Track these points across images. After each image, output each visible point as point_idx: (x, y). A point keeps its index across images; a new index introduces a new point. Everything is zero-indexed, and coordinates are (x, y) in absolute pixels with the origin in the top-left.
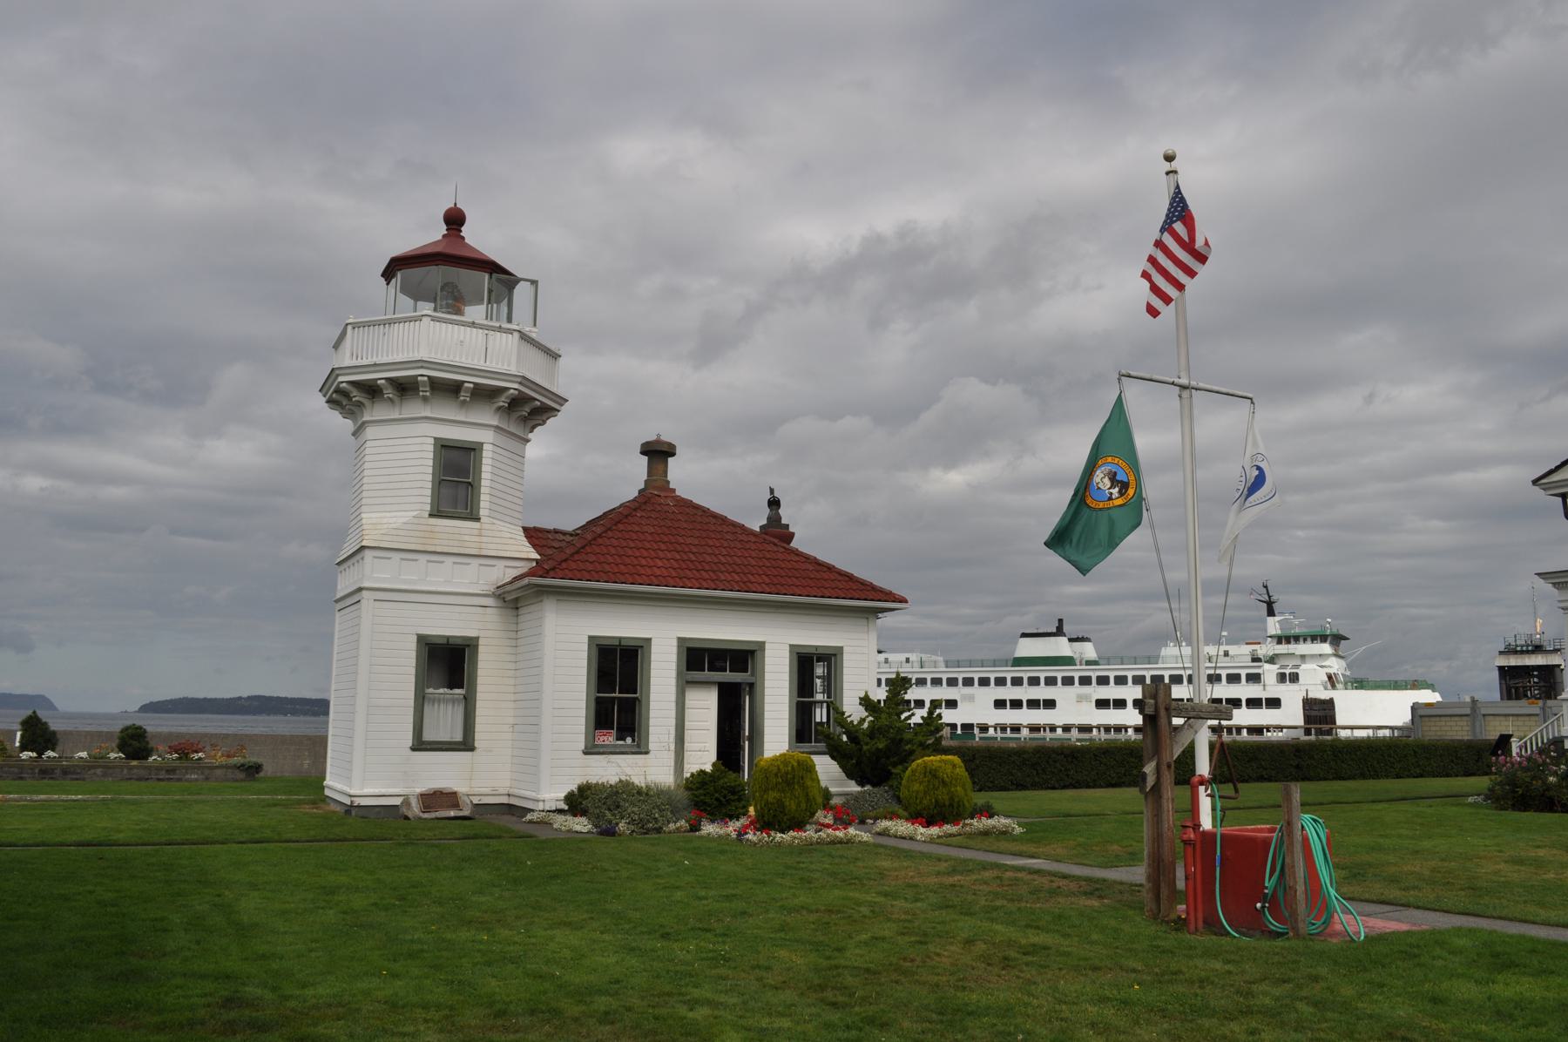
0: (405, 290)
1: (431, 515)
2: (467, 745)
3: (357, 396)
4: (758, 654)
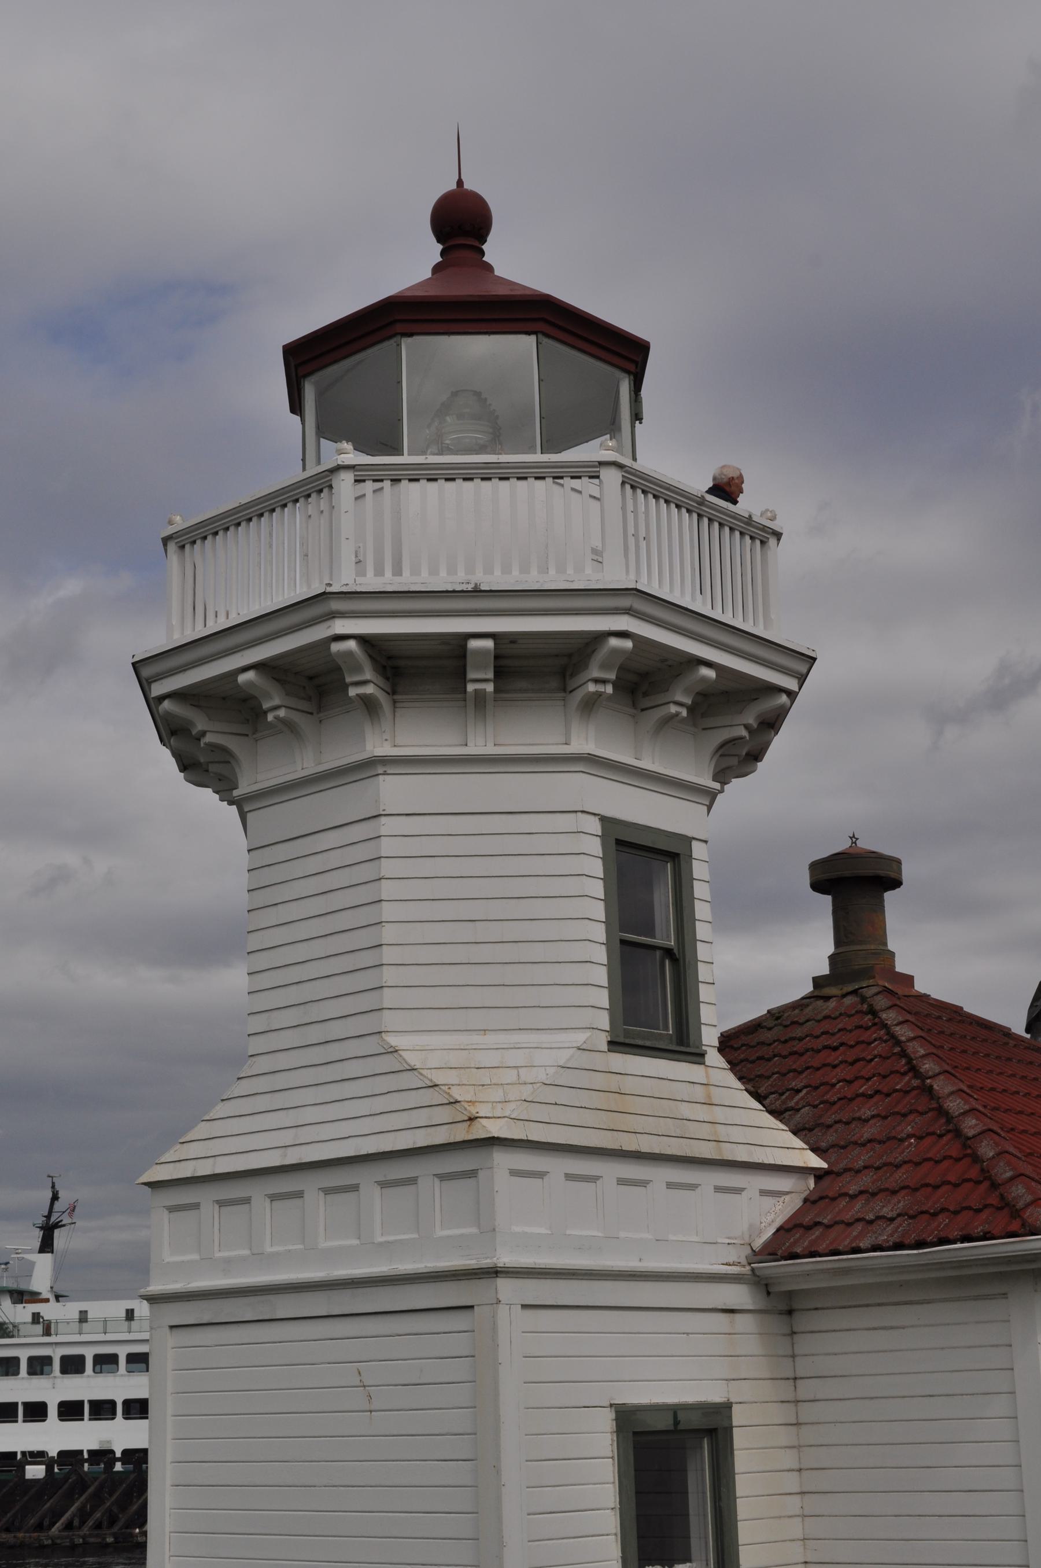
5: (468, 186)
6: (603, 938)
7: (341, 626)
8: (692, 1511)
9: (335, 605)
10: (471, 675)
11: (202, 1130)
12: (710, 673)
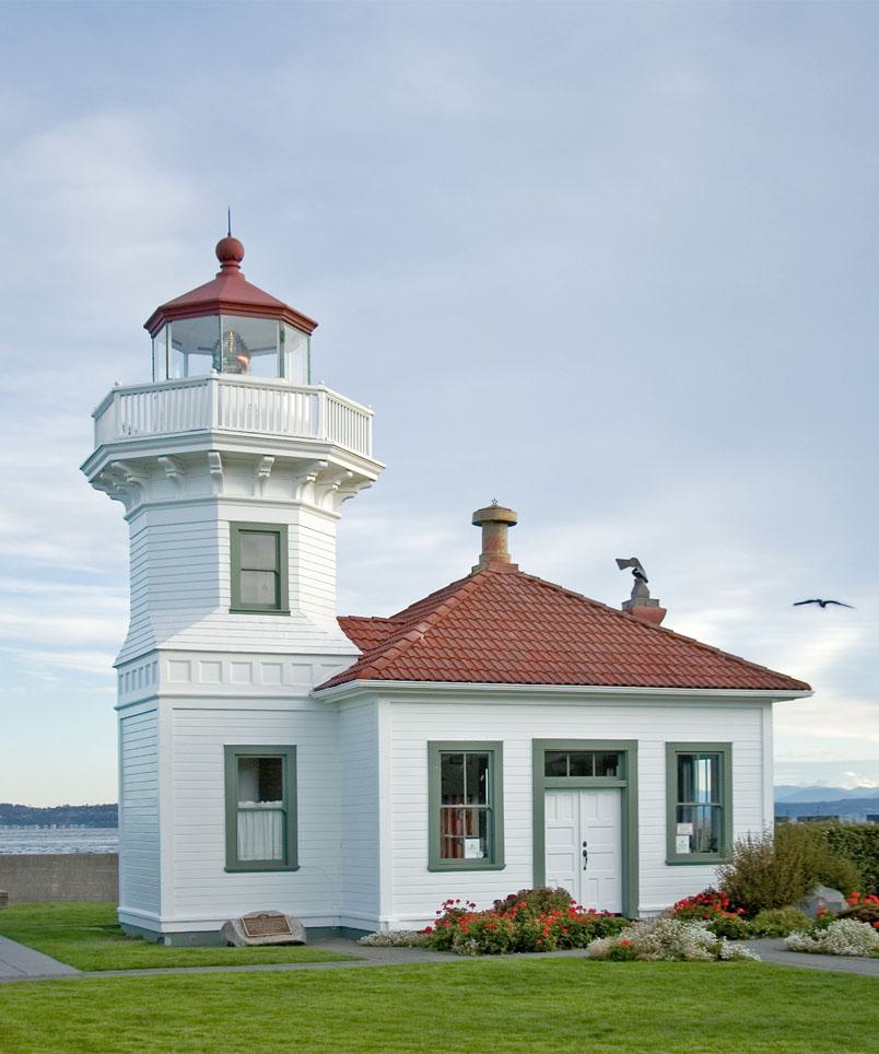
0: (177, 344)
3: (131, 476)
4: (630, 755)
5: (233, 236)
7: (215, 446)
8: (283, 771)
11: (188, 631)
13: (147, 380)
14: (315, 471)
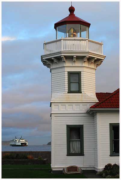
1: (68, 93)
2: (81, 154)
6: (82, 88)
7: (62, 55)
9: (62, 53)
10: (74, 59)
12: (96, 59)
13: (55, 40)
14: (86, 58)
